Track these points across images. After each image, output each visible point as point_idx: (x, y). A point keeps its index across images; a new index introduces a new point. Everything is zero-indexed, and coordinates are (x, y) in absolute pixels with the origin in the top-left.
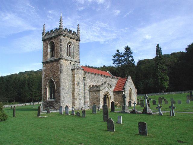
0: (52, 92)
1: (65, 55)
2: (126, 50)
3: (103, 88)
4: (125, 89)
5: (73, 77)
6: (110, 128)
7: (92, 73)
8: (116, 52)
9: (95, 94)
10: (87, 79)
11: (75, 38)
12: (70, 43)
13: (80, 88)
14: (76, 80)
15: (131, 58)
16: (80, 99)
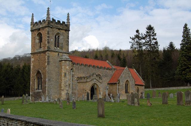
0: (40, 83)
2: (147, 30)
8: (136, 34)
11: (64, 29)
14: (63, 71)
15: (154, 41)
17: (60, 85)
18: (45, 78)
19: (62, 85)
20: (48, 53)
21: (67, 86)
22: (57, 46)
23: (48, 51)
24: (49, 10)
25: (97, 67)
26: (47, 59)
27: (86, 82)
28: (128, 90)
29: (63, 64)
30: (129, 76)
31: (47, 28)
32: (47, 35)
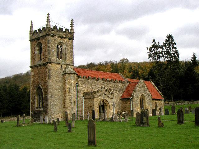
1: (54, 58)
3: (98, 95)
4: (133, 96)
5: (64, 83)
6: (92, 143)
7: (88, 78)
9: (89, 102)
10: (81, 85)
11: (67, 37)
12: (60, 43)
13: (72, 96)
14: (67, 86)
15: (174, 50)
16: (72, 108)
22: (59, 57)
30: (144, 90)
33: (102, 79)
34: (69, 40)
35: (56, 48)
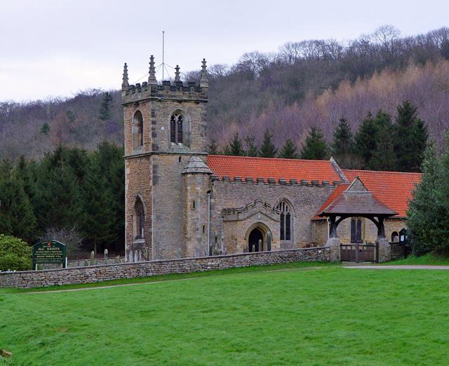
7: (235, 180)
11: (192, 98)
13: (197, 217)
14: (189, 198)
17: (185, 228)
18: (150, 214)
19: (188, 229)
20: (154, 159)
21: (197, 229)
22: (177, 140)
23: (153, 154)
24: (154, 61)
25: (280, 182)
26: (151, 171)
27: (237, 221)
28: (362, 236)
29: (188, 181)
31: (150, 103)
32: (151, 119)
33: (269, 182)
34: (198, 103)
35: (169, 123)
